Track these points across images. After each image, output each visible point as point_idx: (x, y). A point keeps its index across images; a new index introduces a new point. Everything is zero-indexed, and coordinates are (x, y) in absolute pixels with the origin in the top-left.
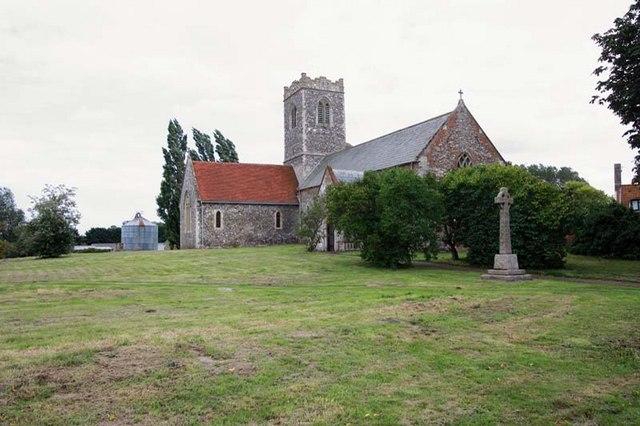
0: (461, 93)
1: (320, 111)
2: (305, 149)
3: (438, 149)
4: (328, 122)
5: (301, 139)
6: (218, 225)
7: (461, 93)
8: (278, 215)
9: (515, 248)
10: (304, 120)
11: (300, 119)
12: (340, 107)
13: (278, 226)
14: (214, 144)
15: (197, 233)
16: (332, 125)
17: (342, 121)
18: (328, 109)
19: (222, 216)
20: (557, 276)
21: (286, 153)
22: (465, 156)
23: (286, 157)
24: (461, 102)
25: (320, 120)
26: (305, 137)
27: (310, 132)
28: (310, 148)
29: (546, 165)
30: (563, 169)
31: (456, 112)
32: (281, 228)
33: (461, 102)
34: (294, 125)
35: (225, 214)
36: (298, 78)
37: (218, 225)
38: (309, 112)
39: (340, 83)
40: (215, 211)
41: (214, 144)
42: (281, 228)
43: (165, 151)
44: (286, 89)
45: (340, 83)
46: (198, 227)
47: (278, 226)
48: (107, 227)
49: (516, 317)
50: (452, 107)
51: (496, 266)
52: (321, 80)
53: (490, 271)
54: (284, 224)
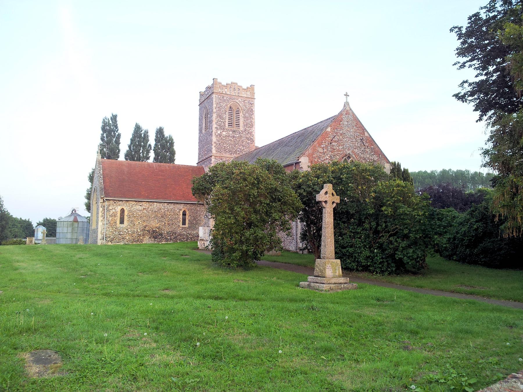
0: (346, 95)
1: (231, 115)
2: (214, 151)
3: (321, 150)
4: (238, 125)
5: (211, 140)
6: (122, 222)
7: (346, 95)
8: (184, 214)
9: (339, 255)
10: (214, 123)
11: (211, 122)
12: (251, 111)
13: (184, 223)
14: (152, 141)
15: (99, 230)
16: (242, 128)
17: (252, 126)
18: (238, 113)
19: (126, 213)
20: (419, 281)
21: (199, 154)
22: (349, 157)
23: (199, 159)
24: (347, 104)
25: (230, 124)
26: (214, 139)
27: (220, 135)
28: (219, 150)
29: (52, 219)
30: (44, 220)
31: (341, 114)
32: (187, 226)
33: (347, 104)
34: (206, 128)
35: (130, 211)
36: (210, 83)
37: (122, 222)
38: (220, 116)
39: (251, 89)
40: (119, 209)
41: (152, 141)
42: (187, 226)
43: (459, 93)
44: (201, 95)
45: (251, 89)
46: (100, 224)
47: (184, 223)
48: (417, 171)
49: (441, 315)
50: (335, 111)
51: (315, 273)
52: (232, 86)
53: (310, 278)
54: (189, 221)
